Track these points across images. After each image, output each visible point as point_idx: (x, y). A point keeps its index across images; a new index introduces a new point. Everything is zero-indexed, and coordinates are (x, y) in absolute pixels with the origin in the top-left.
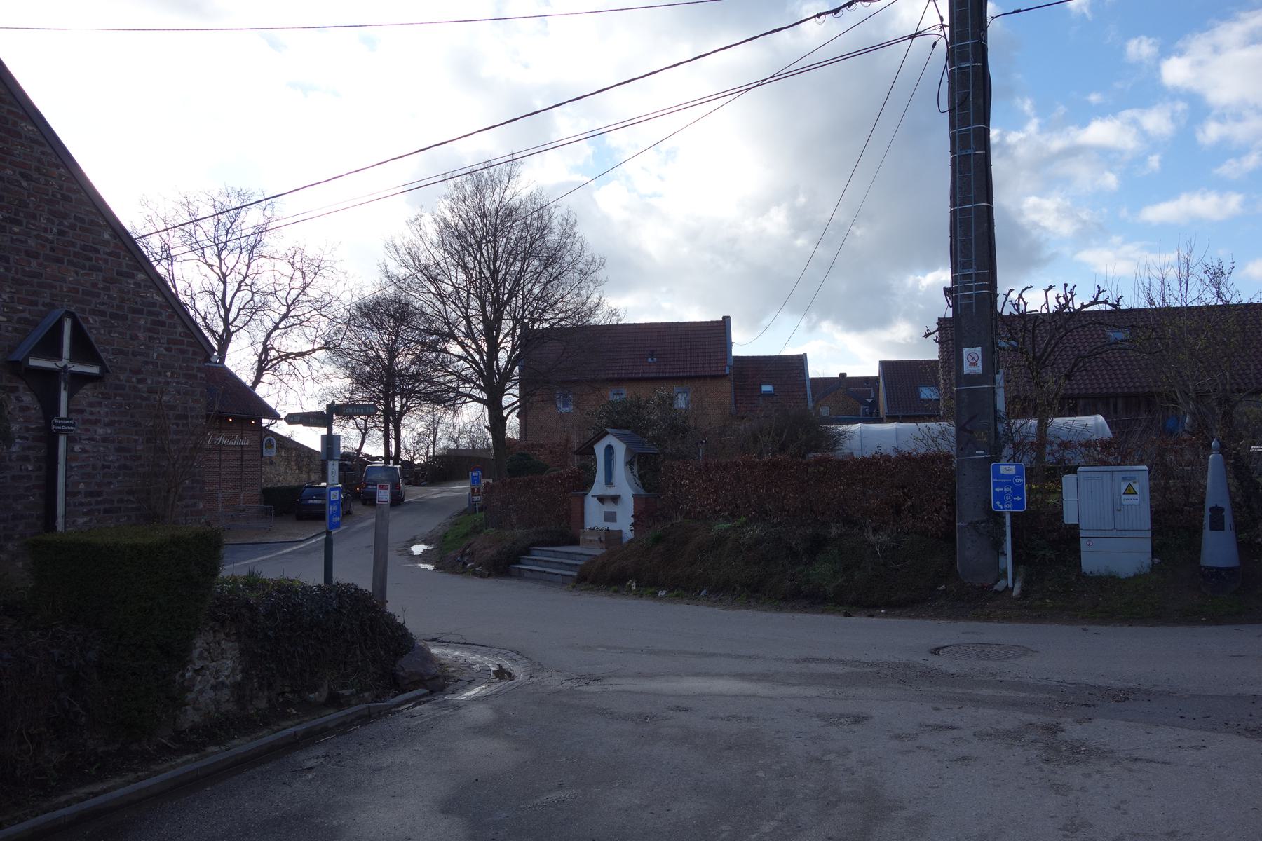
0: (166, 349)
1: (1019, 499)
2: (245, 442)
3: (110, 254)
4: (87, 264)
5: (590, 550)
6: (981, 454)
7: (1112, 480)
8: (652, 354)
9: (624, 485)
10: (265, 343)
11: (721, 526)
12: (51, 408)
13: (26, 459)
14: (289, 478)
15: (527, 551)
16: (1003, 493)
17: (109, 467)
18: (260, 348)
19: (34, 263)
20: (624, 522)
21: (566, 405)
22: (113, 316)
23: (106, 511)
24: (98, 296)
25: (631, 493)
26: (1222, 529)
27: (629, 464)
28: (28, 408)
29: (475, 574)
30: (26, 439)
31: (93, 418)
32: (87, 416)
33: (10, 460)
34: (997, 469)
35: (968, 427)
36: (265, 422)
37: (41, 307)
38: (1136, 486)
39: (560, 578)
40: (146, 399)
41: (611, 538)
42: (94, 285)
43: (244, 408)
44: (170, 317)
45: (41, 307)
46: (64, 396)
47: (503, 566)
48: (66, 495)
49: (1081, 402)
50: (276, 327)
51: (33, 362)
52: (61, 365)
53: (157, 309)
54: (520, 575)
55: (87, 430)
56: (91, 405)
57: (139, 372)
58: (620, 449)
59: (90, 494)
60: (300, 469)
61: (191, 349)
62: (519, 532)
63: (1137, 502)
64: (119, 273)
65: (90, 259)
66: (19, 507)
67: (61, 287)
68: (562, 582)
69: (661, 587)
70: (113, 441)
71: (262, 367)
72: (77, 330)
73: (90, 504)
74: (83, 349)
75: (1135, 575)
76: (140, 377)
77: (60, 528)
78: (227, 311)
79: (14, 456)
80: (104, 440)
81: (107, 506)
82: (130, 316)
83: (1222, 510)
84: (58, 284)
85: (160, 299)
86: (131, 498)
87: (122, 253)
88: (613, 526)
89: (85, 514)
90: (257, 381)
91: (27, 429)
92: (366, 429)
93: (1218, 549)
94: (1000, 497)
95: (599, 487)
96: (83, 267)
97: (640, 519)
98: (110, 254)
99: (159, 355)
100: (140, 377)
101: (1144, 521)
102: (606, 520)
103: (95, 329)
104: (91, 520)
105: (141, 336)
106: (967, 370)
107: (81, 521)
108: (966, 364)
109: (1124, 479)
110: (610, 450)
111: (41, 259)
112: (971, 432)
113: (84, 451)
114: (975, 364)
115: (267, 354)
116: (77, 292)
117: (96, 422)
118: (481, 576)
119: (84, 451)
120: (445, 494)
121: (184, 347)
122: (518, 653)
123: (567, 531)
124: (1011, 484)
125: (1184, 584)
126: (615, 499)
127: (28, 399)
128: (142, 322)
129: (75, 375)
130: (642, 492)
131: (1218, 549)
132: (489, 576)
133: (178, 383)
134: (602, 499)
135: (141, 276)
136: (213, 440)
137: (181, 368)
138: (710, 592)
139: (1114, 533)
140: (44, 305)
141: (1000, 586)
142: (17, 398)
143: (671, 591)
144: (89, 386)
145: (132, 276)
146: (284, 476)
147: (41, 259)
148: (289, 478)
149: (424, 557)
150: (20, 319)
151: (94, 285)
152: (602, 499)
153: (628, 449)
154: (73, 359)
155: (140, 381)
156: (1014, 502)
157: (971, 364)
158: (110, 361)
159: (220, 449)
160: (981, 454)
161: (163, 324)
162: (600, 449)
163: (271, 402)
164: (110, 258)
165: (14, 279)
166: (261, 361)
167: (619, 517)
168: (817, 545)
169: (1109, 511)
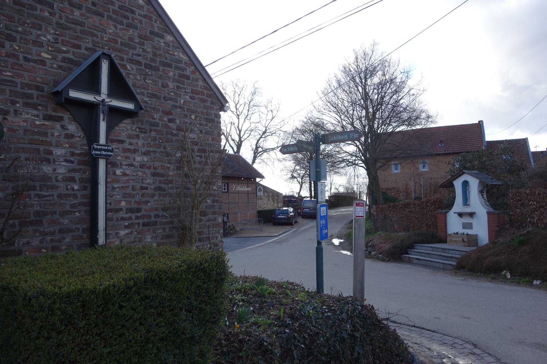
0: (191, 97)
2: (249, 189)
3: (145, 16)
4: (125, 21)
8: (441, 142)
9: (478, 205)
10: (256, 145)
12: (92, 136)
13: (73, 180)
14: (269, 206)
15: (412, 247)
17: (146, 188)
18: (254, 147)
19: (77, 13)
20: (481, 229)
21: (396, 169)
22: (147, 66)
23: (144, 225)
24: (135, 48)
25: (485, 211)
26: (471, 224)
27: (481, 192)
28: (72, 136)
29: (378, 258)
30: (72, 162)
31: (132, 147)
32: (126, 146)
33: (57, 181)
36: (258, 180)
37: (83, 51)
39: (441, 266)
40: (175, 135)
41: (472, 240)
42: (131, 39)
43: (246, 174)
44: (193, 72)
45: (83, 51)
46: (103, 126)
47: (397, 254)
48: (107, 211)
50: (261, 137)
51: (73, 94)
52: (100, 99)
53: (183, 65)
54: (410, 261)
55: (127, 158)
56: (130, 137)
57: (170, 113)
58: (474, 184)
59: (130, 210)
60: (273, 201)
61: (210, 100)
64: (152, 33)
65: (128, 18)
66: (66, 221)
67: (102, 37)
68: (444, 268)
69: (536, 278)
70: (149, 168)
71: (256, 153)
72: (114, 70)
73: (130, 218)
74: (119, 86)
76: (171, 117)
77: (101, 240)
78: (240, 131)
79: (60, 177)
80: (142, 166)
81: (146, 220)
82: (161, 68)
84: (99, 34)
85: (185, 58)
86: (165, 214)
87: (154, 18)
88: (470, 232)
89: (126, 227)
90: (254, 162)
91: (73, 154)
92: (302, 183)
95: (458, 206)
96: (122, 23)
97: (497, 228)
98: (145, 16)
99: (185, 102)
100: (171, 117)
102: (463, 228)
103: (131, 74)
104: (131, 233)
105: (171, 85)
107: (122, 233)
110: (466, 184)
111: (84, 11)
113: (124, 174)
115: (257, 150)
116: (117, 43)
117: (135, 151)
118: (383, 260)
119: (124, 174)
120: (338, 213)
121: (205, 97)
122: (475, 346)
123: (438, 235)
126: (472, 215)
127: (72, 128)
128: (171, 74)
129: (113, 110)
132: (388, 261)
133: (200, 124)
134: (460, 215)
135: (169, 38)
136: (236, 188)
137: (202, 113)
140: (87, 49)
142: (62, 127)
144: (128, 121)
145: (162, 37)
146: (266, 205)
147: (84, 11)
148: (269, 206)
149: (342, 246)
150: (64, 60)
151: (131, 39)
152: (460, 215)
153: (481, 183)
154: (111, 94)
155: (170, 121)
158: (145, 102)
159: (239, 192)
161: (188, 78)
162: (458, 184)
163: (260, 171)
164: (144, 20)
165: (58, 23)
166: (255, 153)
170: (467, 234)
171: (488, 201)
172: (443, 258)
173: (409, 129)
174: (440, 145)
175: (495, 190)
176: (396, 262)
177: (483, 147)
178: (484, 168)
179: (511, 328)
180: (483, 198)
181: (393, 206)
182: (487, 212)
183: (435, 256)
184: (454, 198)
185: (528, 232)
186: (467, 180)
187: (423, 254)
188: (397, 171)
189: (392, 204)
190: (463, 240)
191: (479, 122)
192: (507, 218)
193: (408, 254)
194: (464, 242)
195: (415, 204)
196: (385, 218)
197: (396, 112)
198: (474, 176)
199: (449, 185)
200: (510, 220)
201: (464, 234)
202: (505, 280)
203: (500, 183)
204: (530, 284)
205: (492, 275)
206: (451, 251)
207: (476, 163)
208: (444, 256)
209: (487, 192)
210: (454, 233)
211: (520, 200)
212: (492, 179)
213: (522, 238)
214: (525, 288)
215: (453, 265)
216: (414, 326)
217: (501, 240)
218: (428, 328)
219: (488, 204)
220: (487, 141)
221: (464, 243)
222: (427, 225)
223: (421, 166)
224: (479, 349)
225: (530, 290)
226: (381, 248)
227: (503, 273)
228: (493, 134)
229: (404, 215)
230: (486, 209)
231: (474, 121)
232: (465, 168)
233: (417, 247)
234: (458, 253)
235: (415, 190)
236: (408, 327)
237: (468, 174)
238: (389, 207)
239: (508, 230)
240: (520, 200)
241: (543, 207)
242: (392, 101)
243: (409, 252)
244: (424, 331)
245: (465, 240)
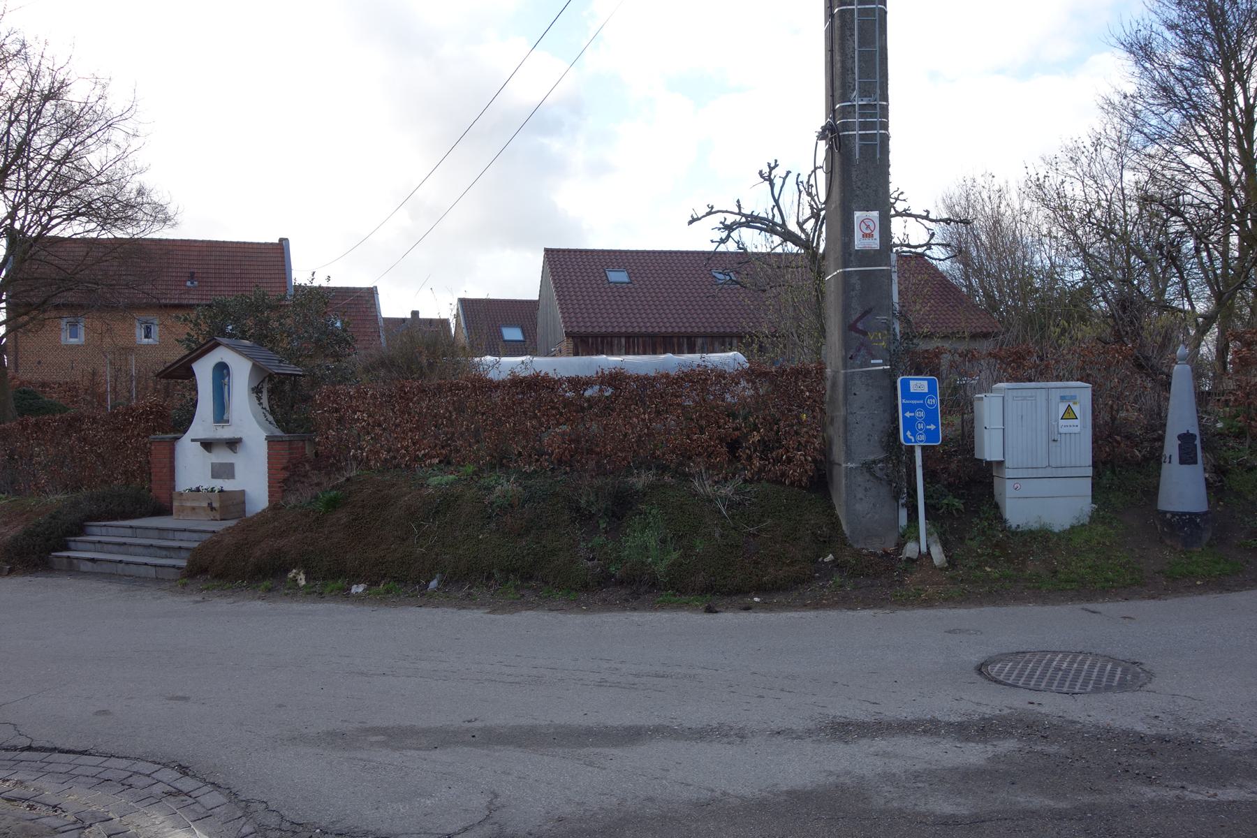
1: (932, 427)
5: (190, 526)
6: (878, 365)
7: (1048, 400)
8: (192, 277)
9: (248, 420)
11: (439, 480)
15: (79, 529)
16: (913, 419)
20: (252, 480)
26: (232, 465)
27: (257, 390)
34: (906, 385)
35: (860, 326)
38: (1076, 408)
39: (152, 571)
41: (232, 503)
49: (699, 341)
54: (72, 568)
58: (241, 370)
62: (57, 498)
63: (1077, 430)
68: (159, 579)
69: (356, 578)
75: (1073, 527)
83: (1193, 437)
88: (228, 485)
93: (1182, 488)
94: (910, 424)
95: (203, 424)
97: (285, 474)
101: (1081, 452)
102: (214, 476)
106: (859, 243)
108: (858, 235)
109: (1063, 398)
110: (222, 370)
112: (864, 333)
114: (870, 236)
122: (184, 770)
123: (149, 496)
124: (923, 406)
125: (1139, 537)
126: (233, 444)
130: (278, 432)
131: (1182, 488)
132: (11, 572)
134: (208, 445)
138: (445, 583)
139: (1049, 472)
141: (911, 550)
143: (373, 583)
152: (208, 445)
153: (256, 368)
156: (927, 432)
157: (865, 236)
160: (878, 365)
162: (203, 370)
167: (238, 471)
168: (622, 506)
169: (1037, 441)
170: (221, 491)
171: (272, 412)
173: (105, 235)
174: (188, 283)
175: (287, 387)
176: (31, 574)
178: (266, 337)
179: (280, 706)
180: (260, 404)
181: (36, 424)
182: (267, 438)
183: (140, 550)
184: (195, 406)
185: (348, 479)
186: (226, 360)
187: (131, 549)
188: (73, 341)
189: (33, 420)
190: (210, 505)
191: (281, 240)
192: (309, 451)
193: (68, 549)
194: (212, 509)
195: (94, 418)
196: (11, 457)
197: (65, 185)
198: (240, 353)
199: (182, 372)
200: (316, 454)
201: (212, 490)
202: (294, 591)
203: (298, 371)
204: (344, 594)
205: (267, 583)
206: (178, 535)
207: (250, 322)
208: (160, 548)
209: (271, 392)
210: (190, 490)
211: (337, 410)
212: (281, 361)
213: (333, 493)
214: (332, 605)
215: (179, 568)
216: (29, 748)
217: (292, 500)
218: (67, 747)
219: (271, 418)
221: (212, 514)
222: (125, 473)
223: (140, 332)
224: (194, 776)
225: (343, 607)
227: (291, 575)
228: (309, 268)
229: (66, 450)
230: (265, 429)
231: (266, 235)
232: (223, 334)
233: (95, 530)
234: (196, 536)
235: (114, 389)
236: (10, 755)
237: (227, 346)
238: (25, 428)
239: (305, 476)
240: (337, 410)
241: (380, 425)
242: (58, 152)
243: (72, 545)
244: (56, 756)
245: (216, 505)
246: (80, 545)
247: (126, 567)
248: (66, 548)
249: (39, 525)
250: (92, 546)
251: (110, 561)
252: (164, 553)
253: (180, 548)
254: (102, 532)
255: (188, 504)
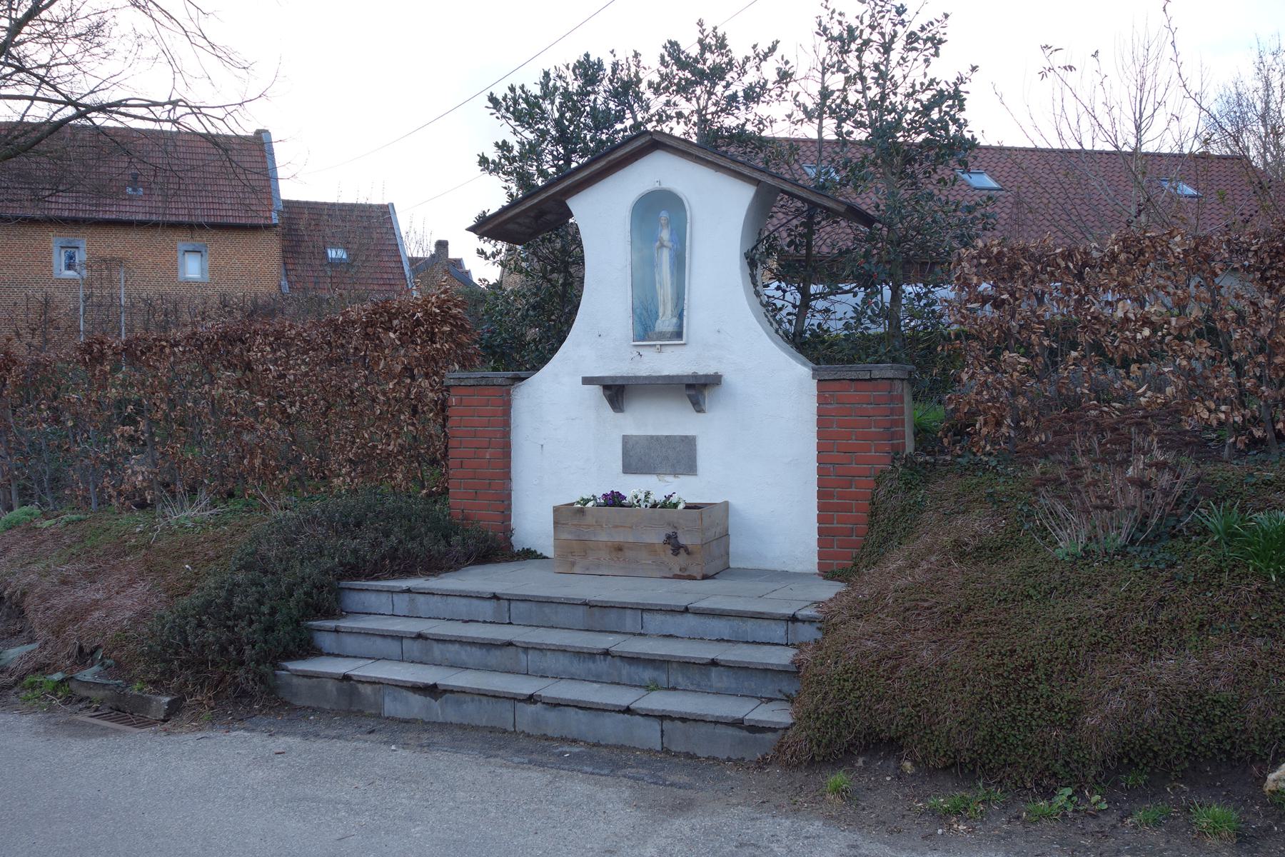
15: (326, 603)
29: (69, 695)
39: (649, 734)
41: (696, 542)
54: (353, 707)
88: (685, 490)
102: (628, 468)
110: (660, 210)
118: (125, 712)
126: (697, 390)
132: (174, 710)
152: (617, 392)
172: (626, 670)
174: (129, 190)
177: (274, 215)
186: (668, 184)
191: (259, 132)
194: (677, 548)
206: (655, 622)
208: (634, 660)
220: (288, 204)
223: (59, 259)
226: (78, 614)
233: (372, 600)
243: (326, 641)
246: (351, 643)
247: (552, 716)
248: (310, 650)
249: (864, 655)
250: (393, 647)
251: (496, 696)
252: (647, 674)
253: (714, 663)
254: (384, 607)
255: (603, 537)
